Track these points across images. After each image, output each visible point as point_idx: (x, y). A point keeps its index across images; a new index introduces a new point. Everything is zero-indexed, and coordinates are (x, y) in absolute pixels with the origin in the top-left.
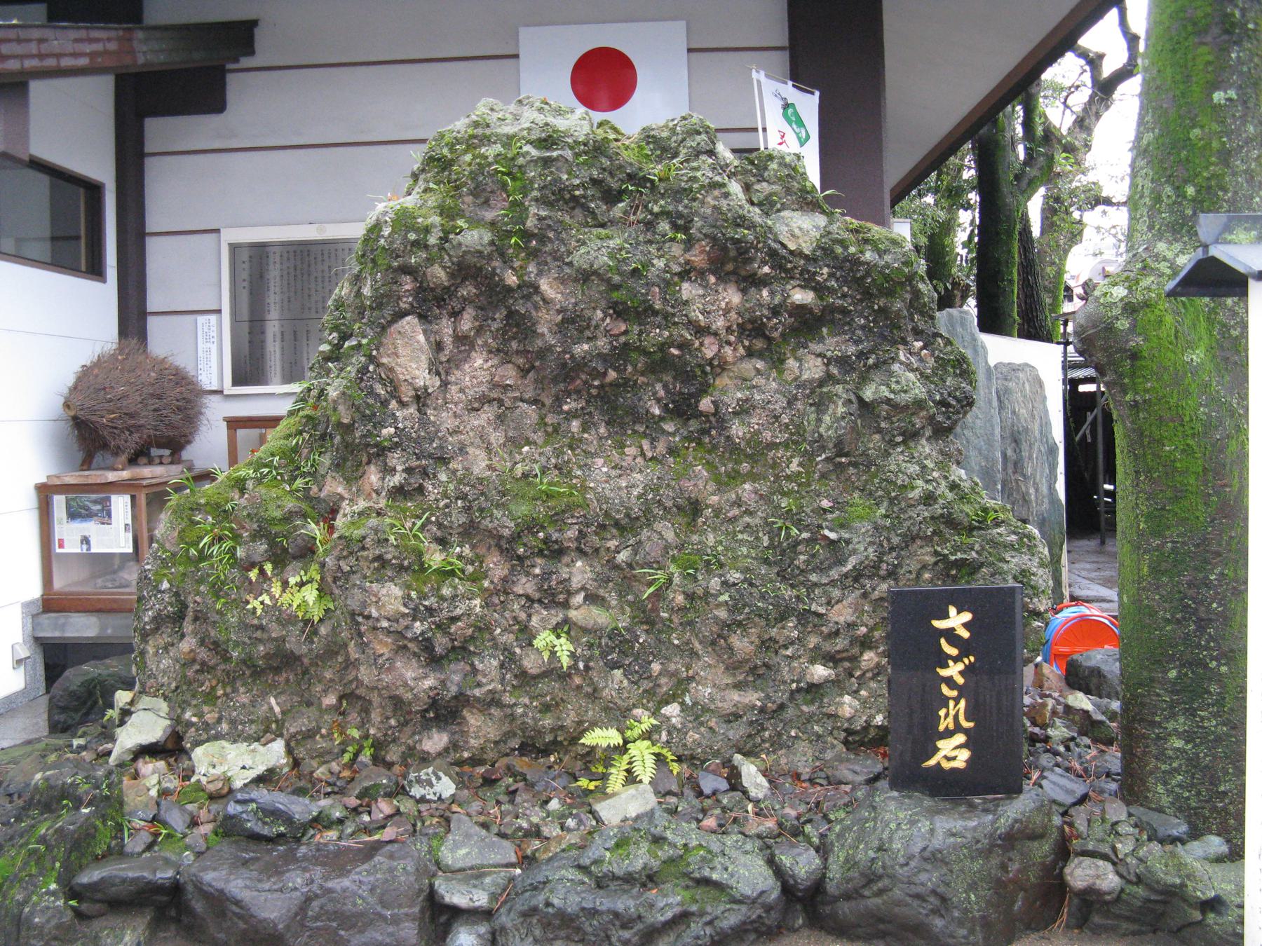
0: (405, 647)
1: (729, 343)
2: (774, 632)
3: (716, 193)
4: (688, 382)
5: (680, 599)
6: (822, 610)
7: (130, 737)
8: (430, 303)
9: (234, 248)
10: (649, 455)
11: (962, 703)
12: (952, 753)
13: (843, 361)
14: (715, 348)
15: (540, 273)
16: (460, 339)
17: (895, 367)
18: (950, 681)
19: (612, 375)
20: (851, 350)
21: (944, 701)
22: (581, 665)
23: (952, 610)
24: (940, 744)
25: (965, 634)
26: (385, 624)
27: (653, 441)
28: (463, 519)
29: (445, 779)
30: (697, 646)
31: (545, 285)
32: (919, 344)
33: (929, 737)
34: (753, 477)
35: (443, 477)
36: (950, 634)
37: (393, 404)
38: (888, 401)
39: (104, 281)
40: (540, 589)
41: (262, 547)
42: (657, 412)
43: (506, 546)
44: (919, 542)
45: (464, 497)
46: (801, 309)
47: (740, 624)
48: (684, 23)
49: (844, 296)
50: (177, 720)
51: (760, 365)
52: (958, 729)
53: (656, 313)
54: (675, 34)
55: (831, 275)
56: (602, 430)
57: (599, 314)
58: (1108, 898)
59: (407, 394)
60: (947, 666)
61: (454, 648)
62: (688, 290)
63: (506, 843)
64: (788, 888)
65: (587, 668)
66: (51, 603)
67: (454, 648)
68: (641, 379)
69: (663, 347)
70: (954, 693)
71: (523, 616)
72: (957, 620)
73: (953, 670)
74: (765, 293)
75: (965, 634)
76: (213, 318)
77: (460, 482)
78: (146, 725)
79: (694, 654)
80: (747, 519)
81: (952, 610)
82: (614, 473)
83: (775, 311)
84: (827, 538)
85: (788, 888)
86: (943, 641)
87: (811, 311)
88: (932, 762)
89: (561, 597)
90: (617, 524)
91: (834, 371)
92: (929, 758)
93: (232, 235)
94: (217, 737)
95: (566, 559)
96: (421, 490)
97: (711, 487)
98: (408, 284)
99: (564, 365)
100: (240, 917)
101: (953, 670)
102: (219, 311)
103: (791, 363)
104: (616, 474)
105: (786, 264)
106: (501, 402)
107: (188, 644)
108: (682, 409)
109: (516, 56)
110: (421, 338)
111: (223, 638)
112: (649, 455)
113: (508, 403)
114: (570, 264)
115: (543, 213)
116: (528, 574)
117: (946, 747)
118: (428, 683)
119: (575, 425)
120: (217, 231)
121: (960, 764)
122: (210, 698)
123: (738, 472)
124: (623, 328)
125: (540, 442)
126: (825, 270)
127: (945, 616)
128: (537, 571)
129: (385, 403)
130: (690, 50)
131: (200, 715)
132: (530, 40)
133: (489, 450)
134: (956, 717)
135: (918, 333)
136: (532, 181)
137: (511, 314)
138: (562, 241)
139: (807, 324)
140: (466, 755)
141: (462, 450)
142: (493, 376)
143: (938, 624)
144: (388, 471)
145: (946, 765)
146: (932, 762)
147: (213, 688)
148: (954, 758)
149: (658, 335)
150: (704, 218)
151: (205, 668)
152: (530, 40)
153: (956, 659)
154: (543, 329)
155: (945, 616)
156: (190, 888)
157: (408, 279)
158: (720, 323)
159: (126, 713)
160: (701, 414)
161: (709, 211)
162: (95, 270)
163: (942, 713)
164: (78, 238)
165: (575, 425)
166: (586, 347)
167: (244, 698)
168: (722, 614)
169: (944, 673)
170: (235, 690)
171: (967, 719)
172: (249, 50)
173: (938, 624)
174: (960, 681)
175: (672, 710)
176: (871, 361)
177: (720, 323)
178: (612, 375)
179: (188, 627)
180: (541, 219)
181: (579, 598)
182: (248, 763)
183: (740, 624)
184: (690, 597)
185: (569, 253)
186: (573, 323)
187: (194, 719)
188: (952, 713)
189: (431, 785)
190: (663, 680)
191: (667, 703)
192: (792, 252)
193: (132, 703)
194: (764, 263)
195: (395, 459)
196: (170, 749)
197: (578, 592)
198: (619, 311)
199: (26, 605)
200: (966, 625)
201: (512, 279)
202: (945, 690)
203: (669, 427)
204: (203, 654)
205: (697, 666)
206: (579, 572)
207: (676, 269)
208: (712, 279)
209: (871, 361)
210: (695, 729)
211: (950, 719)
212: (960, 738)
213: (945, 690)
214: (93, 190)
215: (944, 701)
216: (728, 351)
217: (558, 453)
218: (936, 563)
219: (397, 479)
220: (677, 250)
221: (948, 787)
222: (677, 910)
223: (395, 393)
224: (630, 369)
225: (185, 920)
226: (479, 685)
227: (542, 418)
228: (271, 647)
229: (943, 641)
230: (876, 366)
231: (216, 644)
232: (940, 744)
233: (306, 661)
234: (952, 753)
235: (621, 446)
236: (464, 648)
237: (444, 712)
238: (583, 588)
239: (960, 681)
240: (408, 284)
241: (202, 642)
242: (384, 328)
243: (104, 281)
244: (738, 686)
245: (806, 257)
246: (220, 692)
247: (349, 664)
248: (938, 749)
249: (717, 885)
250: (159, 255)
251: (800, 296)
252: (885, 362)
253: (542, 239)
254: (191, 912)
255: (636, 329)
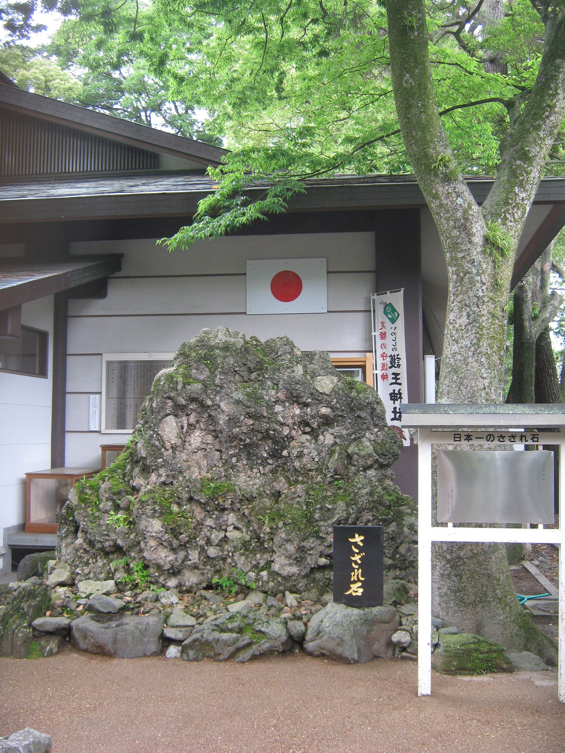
0: (162, 544)
1: (294, 429)
2: (304, 544)
3: (289, 371)
4: (280, 443)
5: (268, 530)
6: (324, 536)
7: (53, 579)
8: (179, 410)
9: (109, 363)
10: (262, 472)
11: (360, 571)
12: (356, 590)
13: (341, 437)
14: (288, 431)
15: (221, 400)
16: (190, 425)
17: (364, 439)
18: (356, 562)
19: (248, 440)
20: (345, 432)
21: (353, 570)
22: (230, 554)
23: (357, 536)
24: (351, 586)
25: (361, 544)
26: (154, 534)
27: (264, 467)
28: (187, 496)
29: (174, 596)
30: (275, 548)
31: (222, 405)
32: (376, 430)
33: (348, 583)
34: (303, 482)
35: (181, 478)
36: (356, 544)
37: (163, 450)
38: (357, 454)
39: (47, 378)
40: (216, 524)
41: (110, 503)
42: (265, 455)
43: (203, 506)
44: (366, 511)
45: (188, 487)
46: (324, 416)
47: (290, 540)
48: (325, 260)
49: (343, 411)
50: (73, 573)
51: (308, 437)
52: (359, 580)
53: (265, 417)
54: (321, 263)
55: (337, 402)
56: (245, 462)
57: (242, 417)
58: (405, 645)
59: (168, 445)
60: (354, 556)
61: (181, 545)
62: (278, 408)
63: (193, 618)
64: (290, 637)
65: (233, 556)
66: (24, 527)
67: (181, 545)
68: (260, 442)
69: (267, 430)
70: (357, 567)
71: (208, 534)
72: (358, 539)
73: (357, 558)
74: (309, 410)
75: (361, 544)
76: (98, 396)
77: (187, 481)
78: (59, 574)
79: (273, 551)
80: (298, 499)
81: (357, 536)
82: (248, 479)
83: (313, 417)
84: (326, 507)
85: (290, 637)
86: (353, 547)
87: (329, 416)
88: (348, 593)
89: (224, 527)
90: (247, 499)
91: (338, 440)
92: (347, 591)
93: (108, 357)
94: (89, 579)
95: (227, 512)
96: (172, 483)
97: (286, 485)
98: (170, 403)
99: (230, 436)
100: (92, 637)
101: (357, 558)
102: (101, 393)
103: (321, 437)
104: (248, 480)
105: (318, 398)
106: (205, 450)
107: (79, 541)
108: (275, 454)
109: (245, 274)
110: (175, 424)
111: (93, 539)
112: (262, 472)
113: (209, 450)
114: (232, 397)
115: (222, 377)
116: (211, 517)
117: (354, 587)
118: (169, 558)
119: (234, 460)
120: (101, 354)
121: (359, 594)
122: (87, 564)
123: (297, 480)
124: (252, 422)
125: (220, 466)
126: (335, 400)
127: (354, 537)
128: (214, 516)
129: (159, 449)
130: (328, 272)
131: (83, 570)
132: (251, 266)
133: (200, 468)
134: (358, 575)
135: (376, 426)
136: (218, 364)
137: (210, 416)
138: (229, 388)
139: (327, 422)
140: (184, 588)
141: (189, 467)
142: (202, 439)
143: (352, 540)
144: (160, 476)
145: (354, 594)
146: (348, 593)
147: (88, 560)
148: (357, 592)
149: (265, 426)
150: (284, 380)
151: (86, 551)
152: (251, 266)
153: (358, 554)
154: (221, 422)
155: (354, 537)
156: (74, 628)
157: (170, 401)
158: (290, 421)
159: (53, 569)
160: (284, 456)
161: (286, 378)
162: (43, 374)
163: (352, 574)
164: (35, 355)
165: (234, 460)
166: (237, 430)
167: (100, 564)
168: (283, 536)
169: (353, 559)
170: (97, 561)
171: (362, 577)
172: (119, 269)
173: (352, 540)
174: (359, 562)
175: (264, 573)
176: (352, 437)
177: (290, 421)
178: (248, 440)
179: (80, 534)
180: (221, 379)
181: (231, 528)
182: (99, 588)
183: (290, 540)
184: (271, 528)
185: (232, 393)
186: (233, 421)
187: (80, 572)
188: (356, 574)
189: (169, 598)
190: (261, 561)
191: (262, 571)
192: (321, 393)
193: (55, 565)
194: (309, 398)
195: (162, 471)
196: (71, 584)
197: (230, 525)
198: (250, 416)
199: (7, 530)
200: (361, 541)
201: (209, 403)
202: (354, 565)
203: (270, 461)
204: (85, 546)
205: (275, 557)
206: (231, 518)
207: (273, 400)
208: (287, 404)
209: (352, 437)
210: (273, 581)
211: (356, 576)
212: (360, 584)
213: (354, 565)
214: (44, 335)
215: (353, 570)
216: (294, 432)
217: (226, 470)
218: (374, 519)
219: (163, 479)
220: (273, 392)
221: (352, 602)
222: (248, 641)
223: (163, 446)
224: (255, 438)
225: (72, 642)
226: (190, 560)
227: (221, 456)
228: (111, 543)
229: (353, 547)
230: (355, 439)
231: (90, 541)
232: (351, 586)
233: (124, 549)
234: (356, 590)
235: (251, 469)
236: (185, 545)
237: (175, 572)
238: (233, 524)
239: (359, 562)
240: (170, 403)
241: (85, 540)
242: (161, 420)
243: (47, 378)
244: (290, 565)
245: (327, 395)
246: (90, 561)
247: (141, 551)
248: (350, 588)
249: (263, 633)
250: (74, 366)
251: (324, 410)
252: (359, 438)
253: (222, 387)
254: (74, 639)
255: (257, 423)
